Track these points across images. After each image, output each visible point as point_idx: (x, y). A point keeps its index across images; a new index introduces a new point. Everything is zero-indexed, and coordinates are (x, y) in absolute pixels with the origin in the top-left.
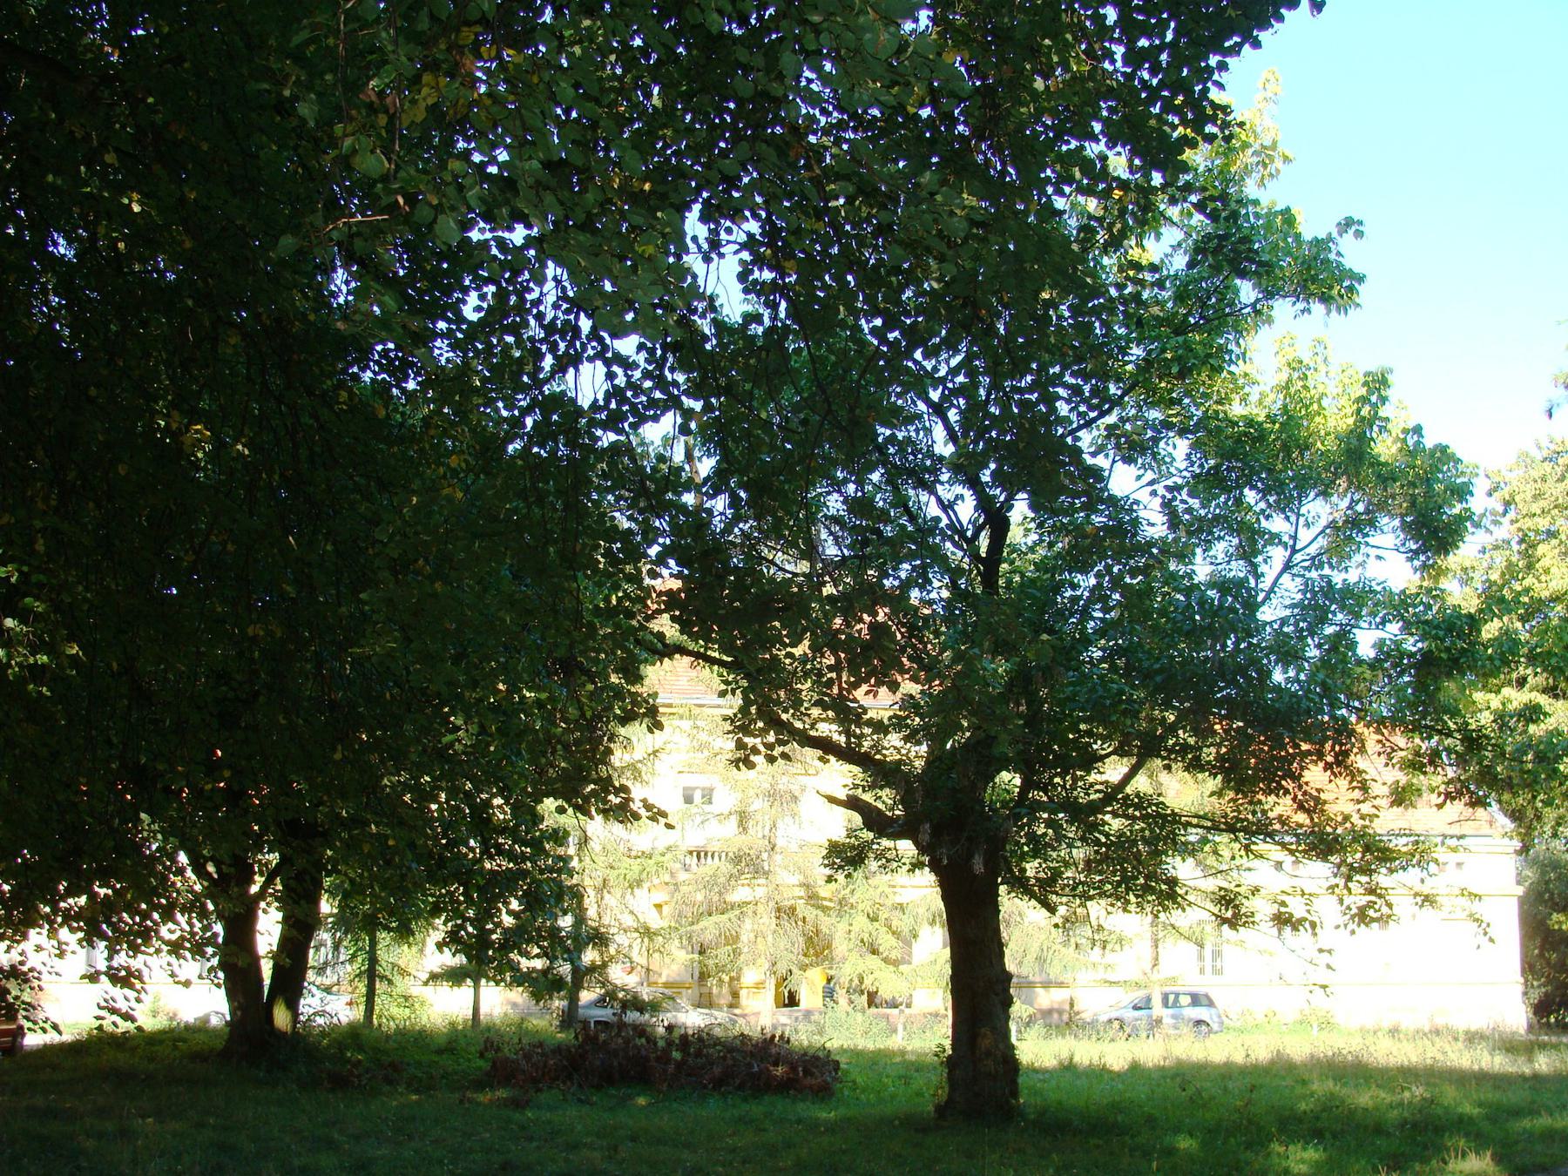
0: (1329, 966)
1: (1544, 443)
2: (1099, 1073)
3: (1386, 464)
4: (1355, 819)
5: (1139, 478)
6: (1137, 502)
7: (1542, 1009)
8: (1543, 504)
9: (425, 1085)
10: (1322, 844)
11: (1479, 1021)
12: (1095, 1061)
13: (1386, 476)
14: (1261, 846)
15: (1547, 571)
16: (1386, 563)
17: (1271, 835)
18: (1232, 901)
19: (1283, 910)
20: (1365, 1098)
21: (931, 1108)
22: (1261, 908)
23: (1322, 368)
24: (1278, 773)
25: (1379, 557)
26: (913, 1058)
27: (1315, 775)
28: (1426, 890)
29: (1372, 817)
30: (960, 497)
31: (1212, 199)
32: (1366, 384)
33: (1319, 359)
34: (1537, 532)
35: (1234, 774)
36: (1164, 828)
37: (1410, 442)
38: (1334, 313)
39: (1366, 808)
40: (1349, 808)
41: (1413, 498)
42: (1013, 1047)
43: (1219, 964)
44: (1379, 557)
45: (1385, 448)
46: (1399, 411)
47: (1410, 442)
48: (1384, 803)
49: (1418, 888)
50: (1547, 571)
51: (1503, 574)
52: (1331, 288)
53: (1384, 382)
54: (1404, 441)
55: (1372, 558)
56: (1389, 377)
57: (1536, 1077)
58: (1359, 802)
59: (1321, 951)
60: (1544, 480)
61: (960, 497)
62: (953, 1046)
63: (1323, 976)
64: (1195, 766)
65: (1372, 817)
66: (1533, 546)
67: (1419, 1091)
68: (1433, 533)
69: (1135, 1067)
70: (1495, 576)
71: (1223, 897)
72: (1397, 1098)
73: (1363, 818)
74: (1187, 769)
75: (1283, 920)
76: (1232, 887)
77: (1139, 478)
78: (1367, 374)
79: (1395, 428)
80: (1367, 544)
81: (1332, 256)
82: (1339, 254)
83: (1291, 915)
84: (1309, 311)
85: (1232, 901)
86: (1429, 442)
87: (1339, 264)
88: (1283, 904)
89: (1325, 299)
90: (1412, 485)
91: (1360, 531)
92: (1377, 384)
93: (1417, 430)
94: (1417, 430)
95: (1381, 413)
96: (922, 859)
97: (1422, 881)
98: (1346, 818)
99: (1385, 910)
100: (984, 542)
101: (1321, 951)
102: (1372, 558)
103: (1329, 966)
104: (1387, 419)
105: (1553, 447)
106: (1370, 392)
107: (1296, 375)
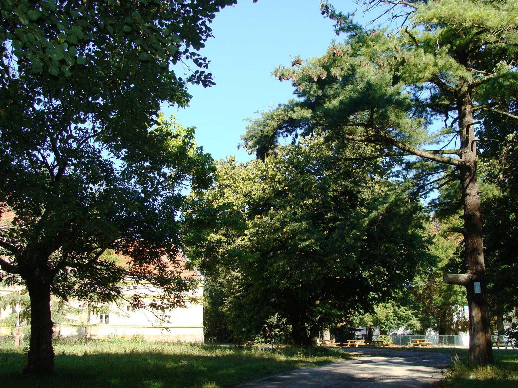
0: (168, 322)
1: (229, 157)
2: (74, 357)
3: (191, 158)
4: (175, 273)
5: (109, 155)
6: (112, 162)
7: (206, 336)
8: (227, 176)
9: (430, 352)
10: (161, 281)
11: (189, 340)
12: (72, 353)
13: (191, 161)
14: (143, 281)
15: (227, 197)
16: (186, 190)
17: (146, 277)
18: (138, 299)
19: (153, 302)
20: (170, 365)
21: (21, 371)
22: (147, 301)
23: (173, 125)
24: (154, 256)
25: (186, 188)
26: (5, 352)
27: (165, 258)
28: (193, 297)
29: (180, 273)
30: (49, 155)
31: (201, 59)
32: (187, 131)
33: (172, 122)
34: (225, 185)
35: (139, 257)
36: (118, 274)
37: (199, 152)
38: (180, 107)
39: (179, 270)
40: (173, 269)
41: (198, 170)
42: (52, 348)
43: (107, 320)
44: (186, 188)
45: (191, 153)
46: (198, 141)
47: (199, 152)
48: (183, 268)
49: (191, 296)
50: (227, 197)
51: (213, 197)
52: (181, 99)
53: (193, 132)
54: (197, 151)
55: (184, 188)
56: (195, 130)
57: (217, 357)
58: (176, 267)
59: (166, 316)
60: (228, 168)
61: (49, 155)
62: (31, 348)
63: (166, 325)
64: (126, 253)
65: (180, 273)
66: (223, 189)
67: (184, 363)
68: (202, 182)
69: (86, 354)
70: (210, 198)
71: (135, 298)
72: (177, 365)
73: (177, 273)
74: (123, 254)
75: (153, 305)
76: (138, 294)
77: (109, 155)
78: (188, 128)
79: (195, 147)
80: (182, 184)
81: (184, 89)
82: (186, 88)
83: (156, 304)
84: (173, 106)
85: (138, 299)
86: (205, 153)
87: (186, 91)
88: (154, 300)
89: (179, 102)
90: (198, 166)
91: (180, 179)
92: (191, 132)
93: (201, 148)
94: (201, 148)
95: (191, 141)
96: (23, 281)
97: (193, 294)
98: (172, 272)
99: (182, 303)
100: (56, 171)
101: (166, 316)
102: (184, 188)
103: (168, 322)
104: (193, 144)
105: (231, 159)
106: (188, 134)
107: (164, 126)
